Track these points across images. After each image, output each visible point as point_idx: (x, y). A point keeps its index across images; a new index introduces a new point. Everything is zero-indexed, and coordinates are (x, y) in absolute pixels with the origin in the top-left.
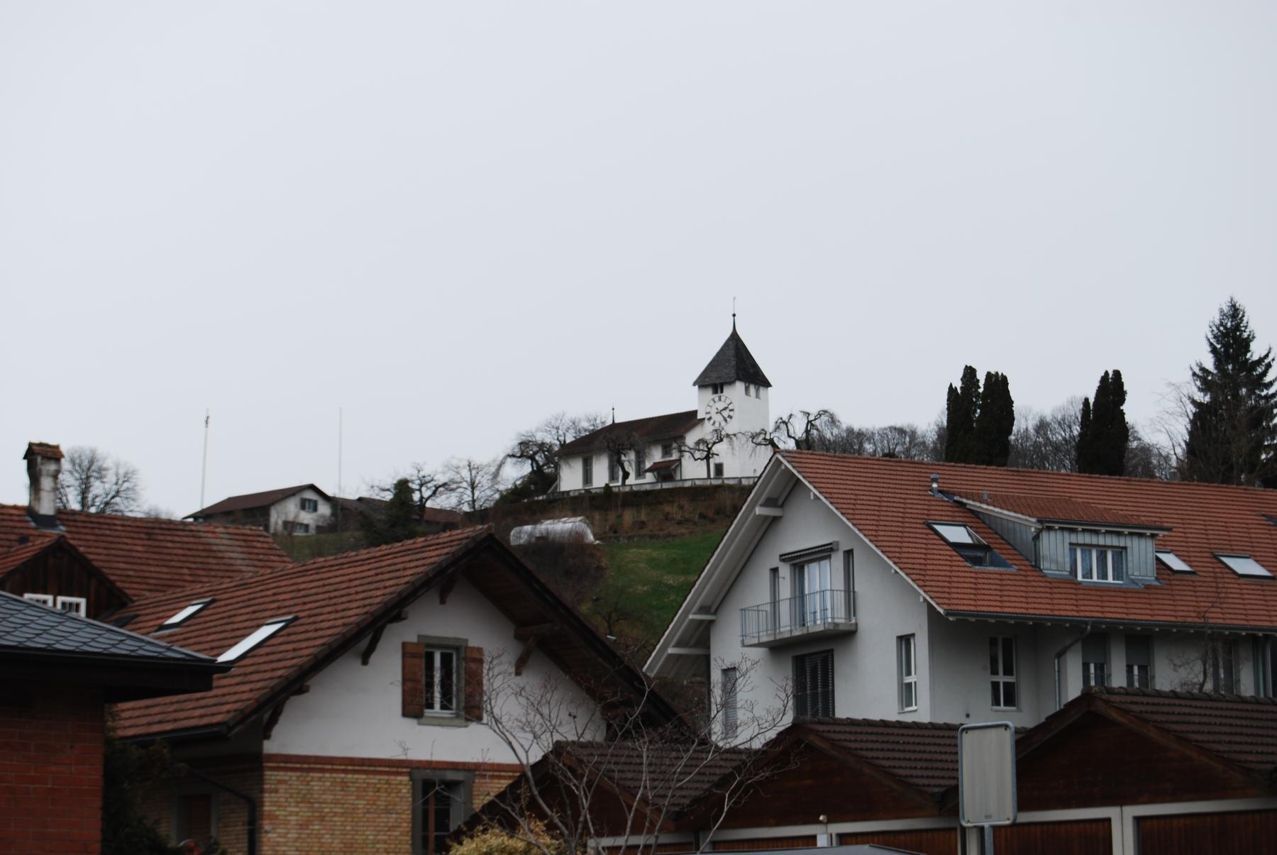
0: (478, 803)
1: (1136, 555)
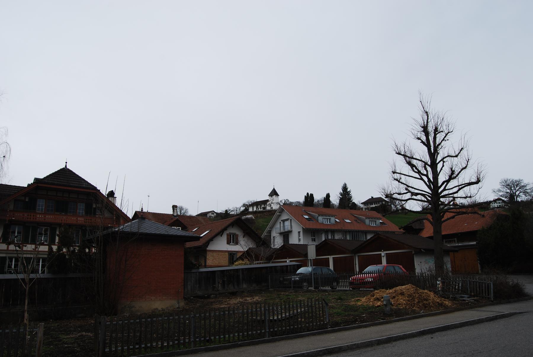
0: (238, 257)
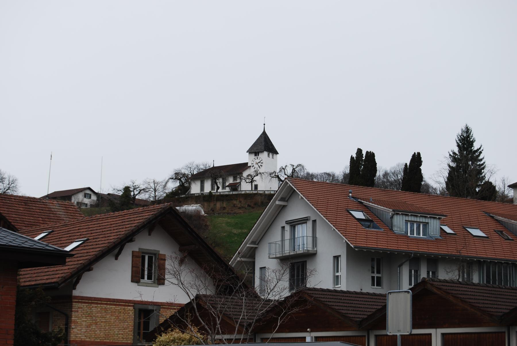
0: (162, 320)
1: (432, 226)
